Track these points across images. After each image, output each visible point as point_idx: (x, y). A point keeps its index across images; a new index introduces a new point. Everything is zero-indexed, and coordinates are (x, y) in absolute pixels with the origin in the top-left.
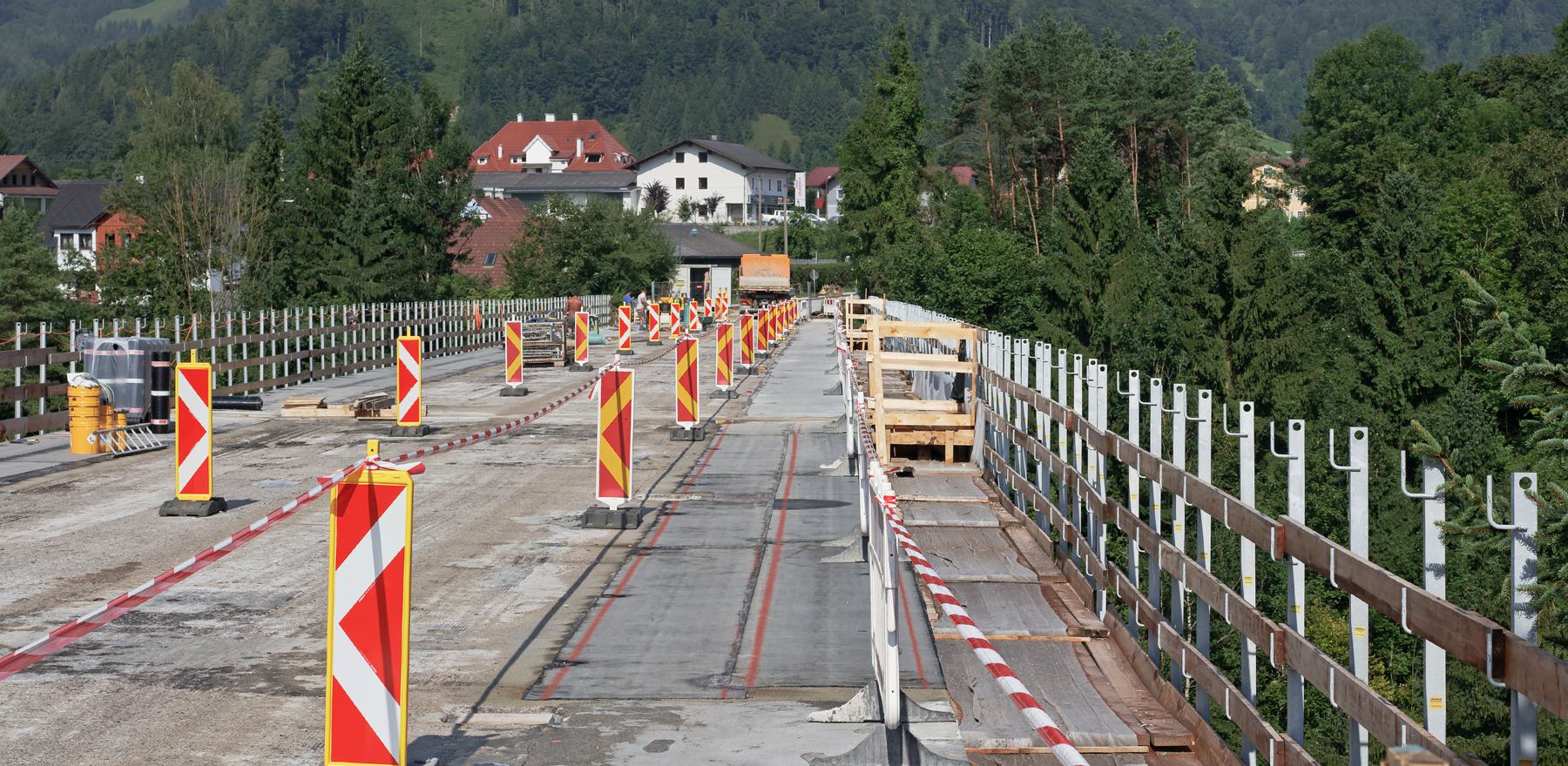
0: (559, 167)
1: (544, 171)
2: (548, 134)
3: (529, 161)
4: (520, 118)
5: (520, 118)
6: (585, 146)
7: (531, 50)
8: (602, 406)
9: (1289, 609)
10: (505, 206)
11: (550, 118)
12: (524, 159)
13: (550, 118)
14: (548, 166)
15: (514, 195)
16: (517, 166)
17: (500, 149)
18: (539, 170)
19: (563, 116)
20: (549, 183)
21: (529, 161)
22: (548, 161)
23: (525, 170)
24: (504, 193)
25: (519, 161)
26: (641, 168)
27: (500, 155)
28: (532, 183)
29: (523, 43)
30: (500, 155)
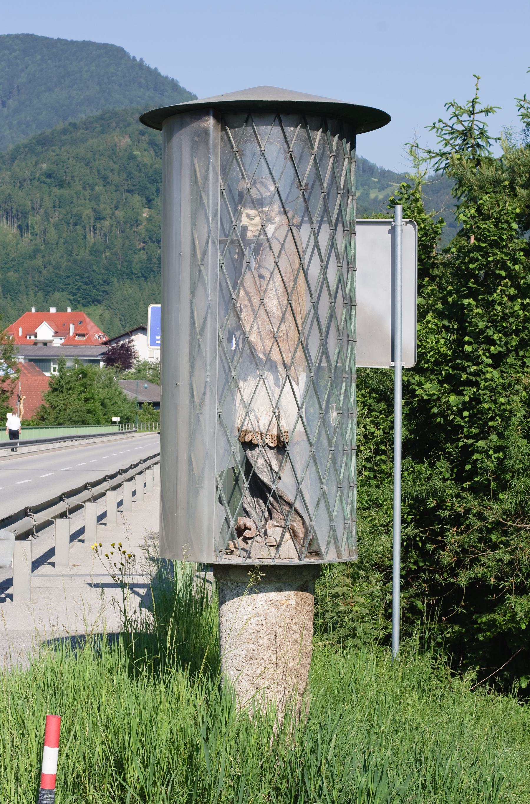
0: (58, 342)
1: (48, 344)
2: (51, 320)
3: (39, 337)
4: (33, 310)
5: (33, 310)
6: (76, 329)
7: (39, 262)
8: (228, 504)
9: (278, 585)
10: (25, 368)
11: (53, 310)
12: (36, 337)
13: (53, 310)
14: (51, 341)
15: (30, 360)
16: (31, 341)
17: (20, 330)
18: (45, 344)
19: (61, 309)
20: (52, 353)
21: (39, 337)
22: (50, 338)
23: (36, 344)
24: (25, 359)
25: (33, 338)
26: (353, 295)
27: (20, 334)
28: (40, 353)
29: (32, 257)
30: (20, 334)
